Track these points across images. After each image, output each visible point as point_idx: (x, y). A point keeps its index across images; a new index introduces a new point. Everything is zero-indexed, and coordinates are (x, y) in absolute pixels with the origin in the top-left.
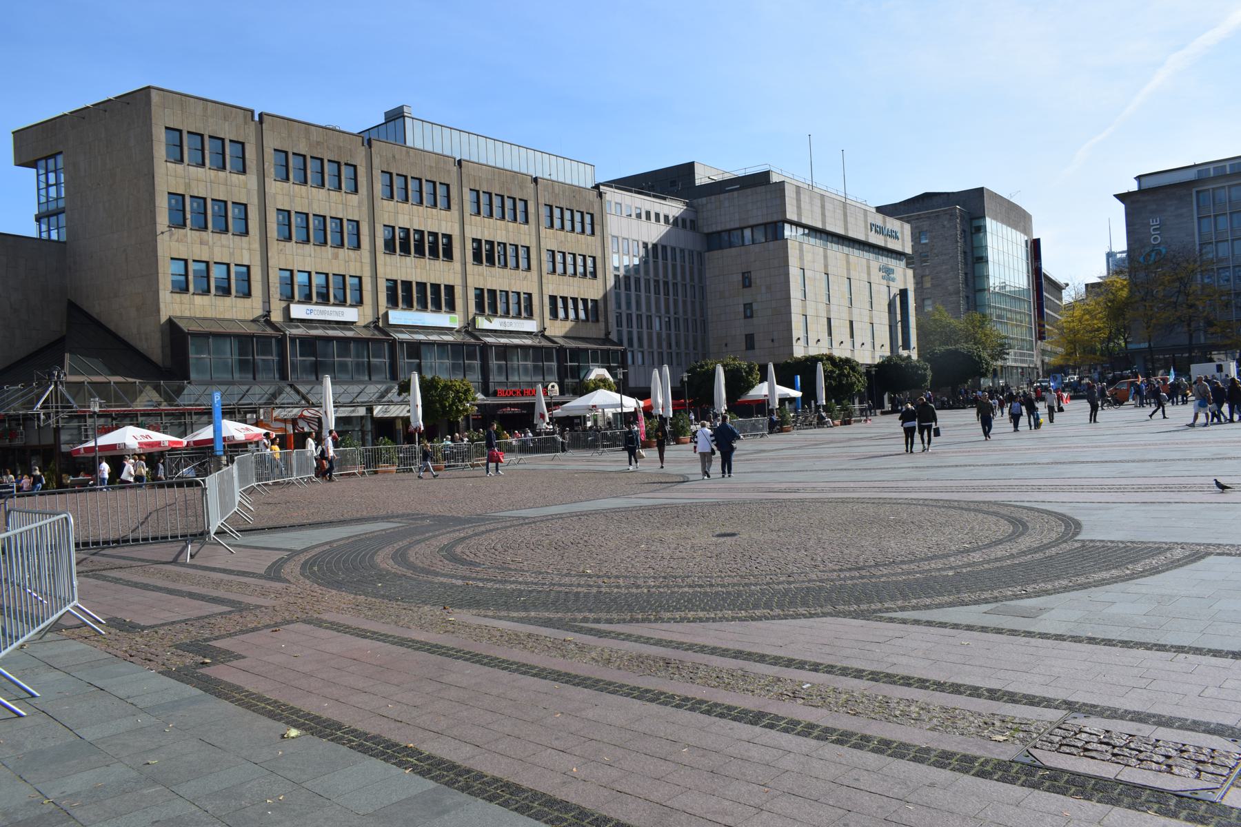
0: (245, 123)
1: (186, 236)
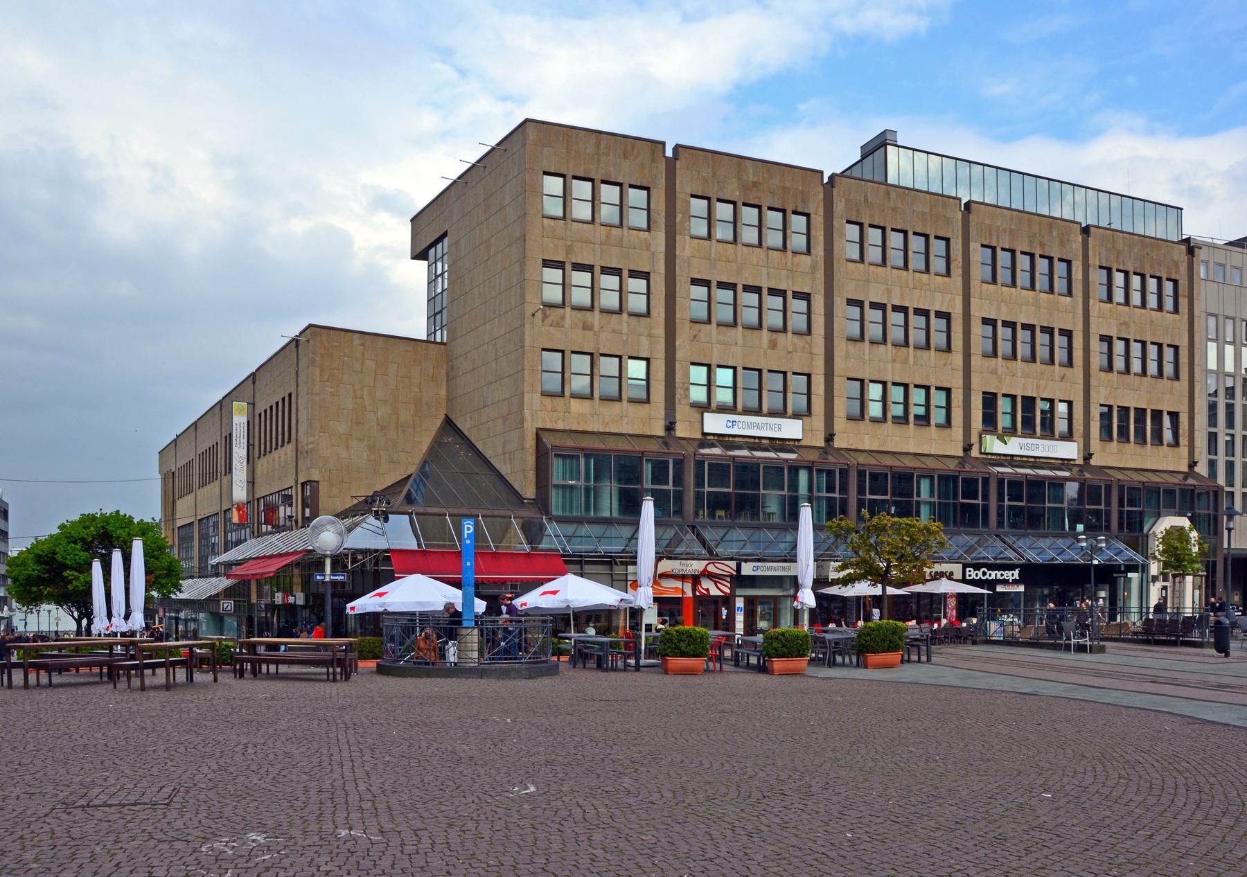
0: (653, 160)
1: (563, 318)
